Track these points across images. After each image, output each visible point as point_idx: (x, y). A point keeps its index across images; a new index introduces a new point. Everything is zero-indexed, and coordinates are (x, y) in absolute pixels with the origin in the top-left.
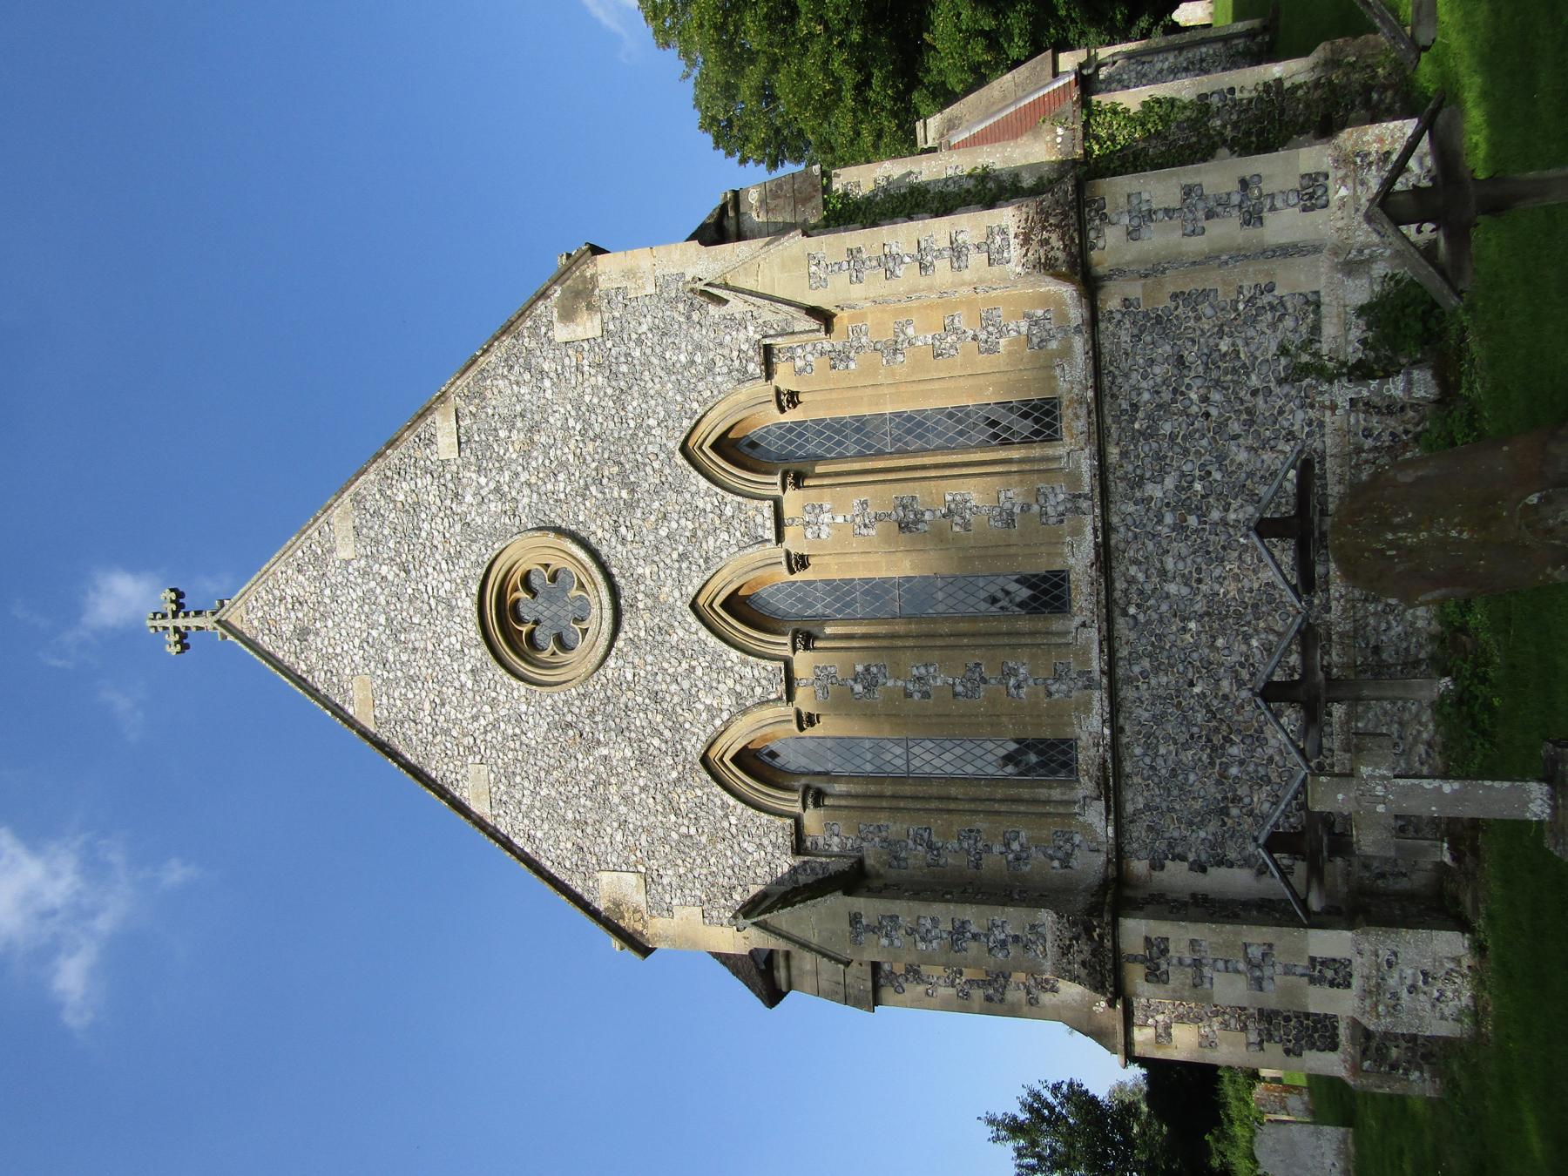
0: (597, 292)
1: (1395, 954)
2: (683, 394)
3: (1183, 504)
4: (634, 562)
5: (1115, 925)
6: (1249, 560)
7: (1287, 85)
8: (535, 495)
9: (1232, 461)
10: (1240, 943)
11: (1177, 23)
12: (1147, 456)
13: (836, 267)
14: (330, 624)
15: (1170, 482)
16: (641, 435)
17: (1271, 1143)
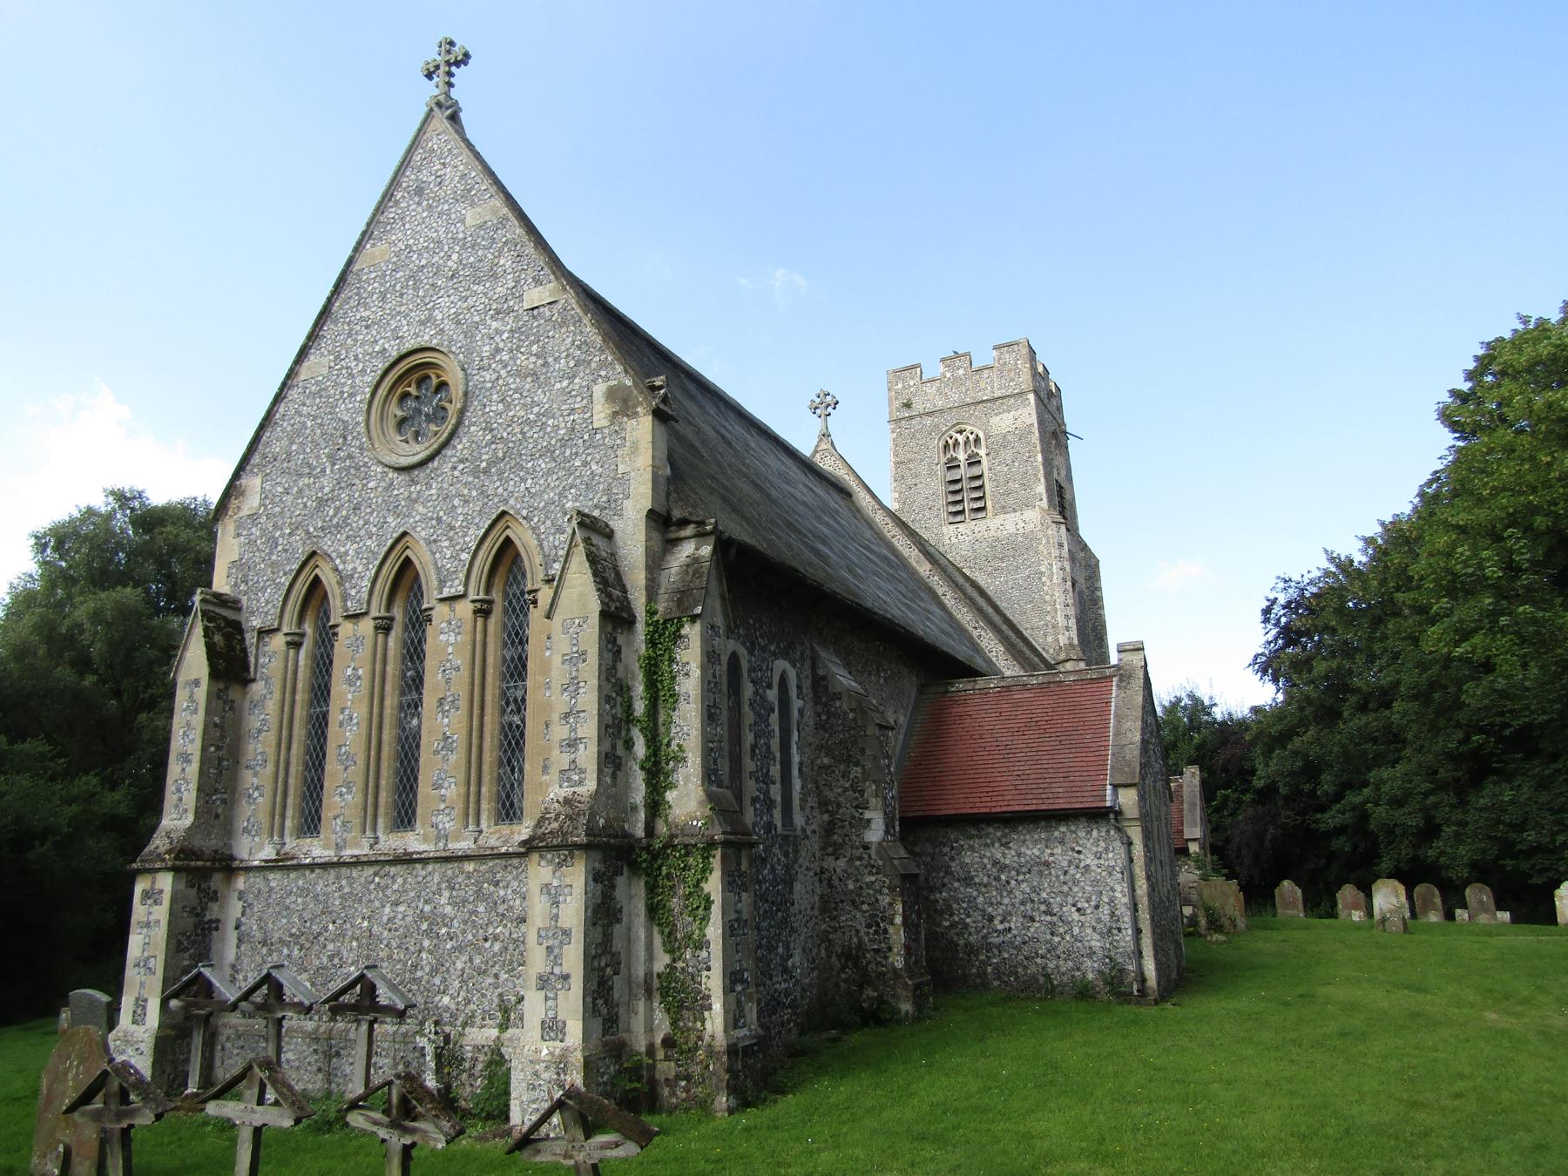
0: (625, 419)
1: (142, 1054)
2: (544, 507)
3: (436, 919)
4: (440, 479)
5: (168, 869)
6: (398, 967)
7: (706, 1014)
8: (490, 385)
9: (457, 957)
10: (157, 953)
11: (1559, 887)
12: (466, 892)
14: (425, 214)
15: (448, 909)
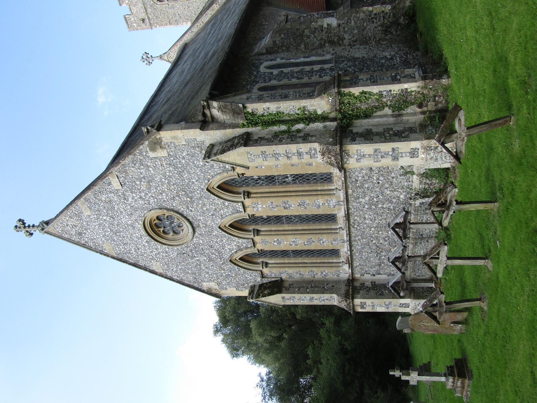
0: (163, 143)
3: (371, 203)
7: (409, 90)
9: (385, 194)
13: (258, 156)
15: (367, 198)
16: (191, 184)
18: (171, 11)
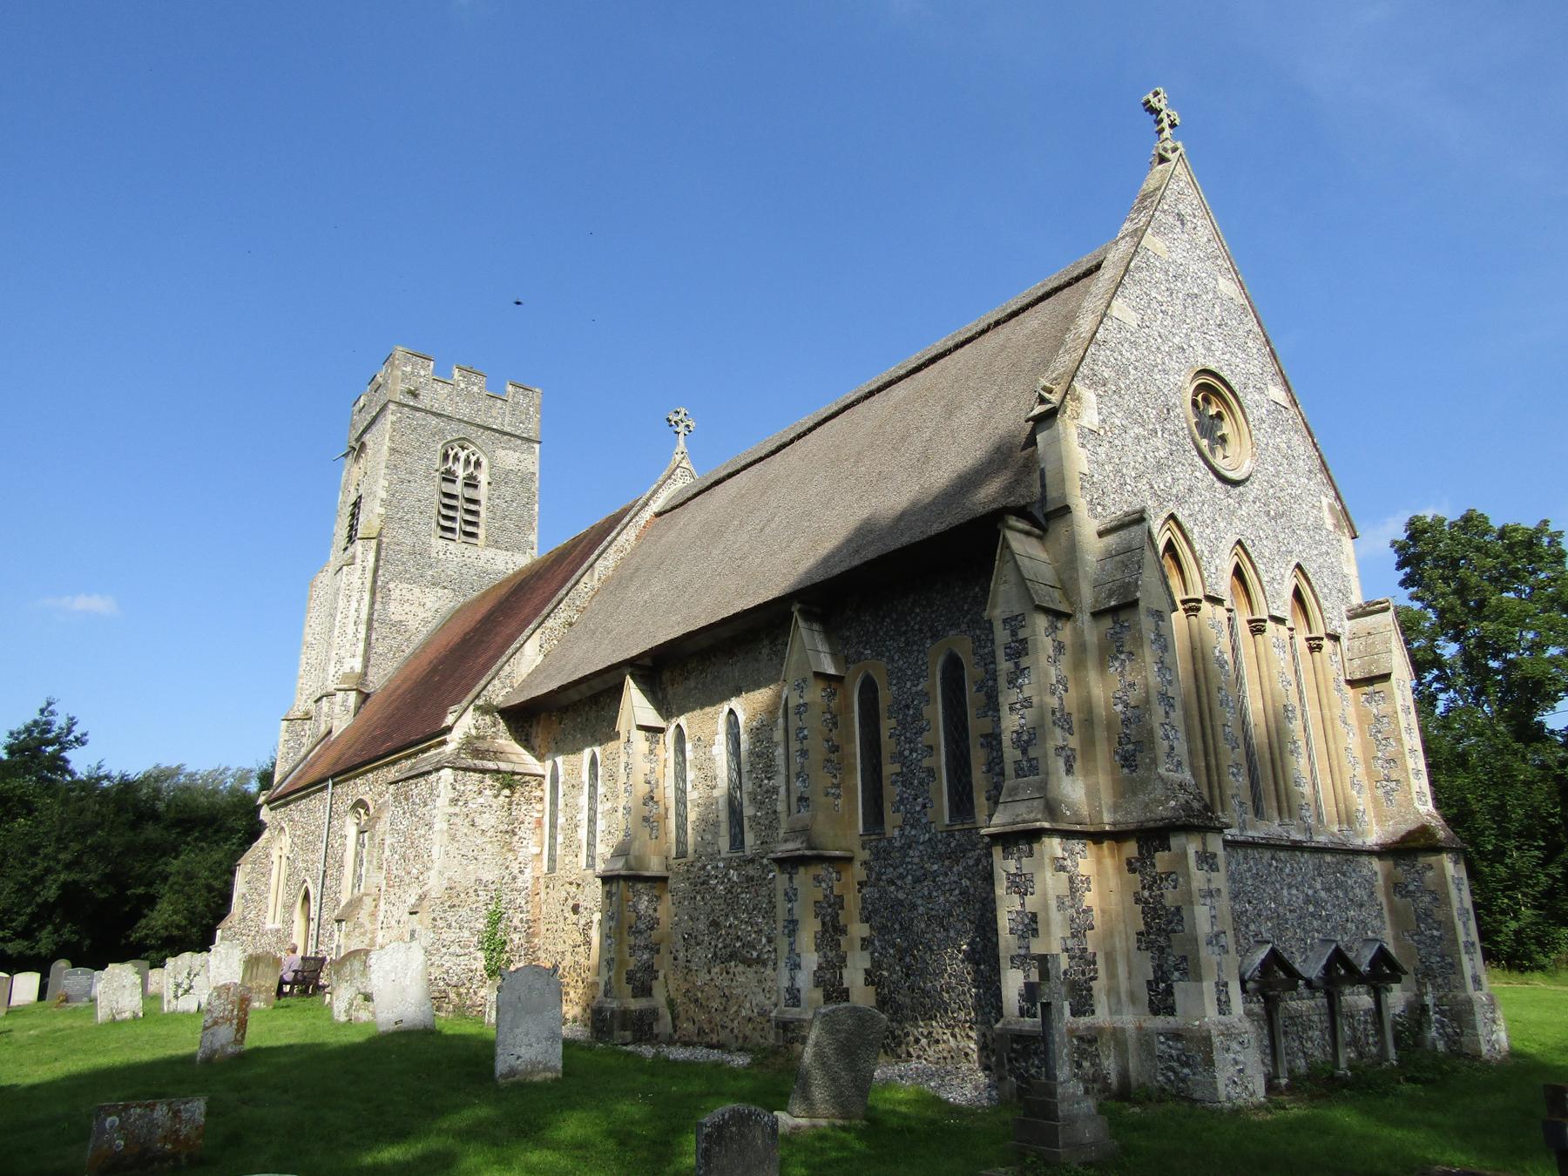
17: (538, 986)
18: (420, 467)
